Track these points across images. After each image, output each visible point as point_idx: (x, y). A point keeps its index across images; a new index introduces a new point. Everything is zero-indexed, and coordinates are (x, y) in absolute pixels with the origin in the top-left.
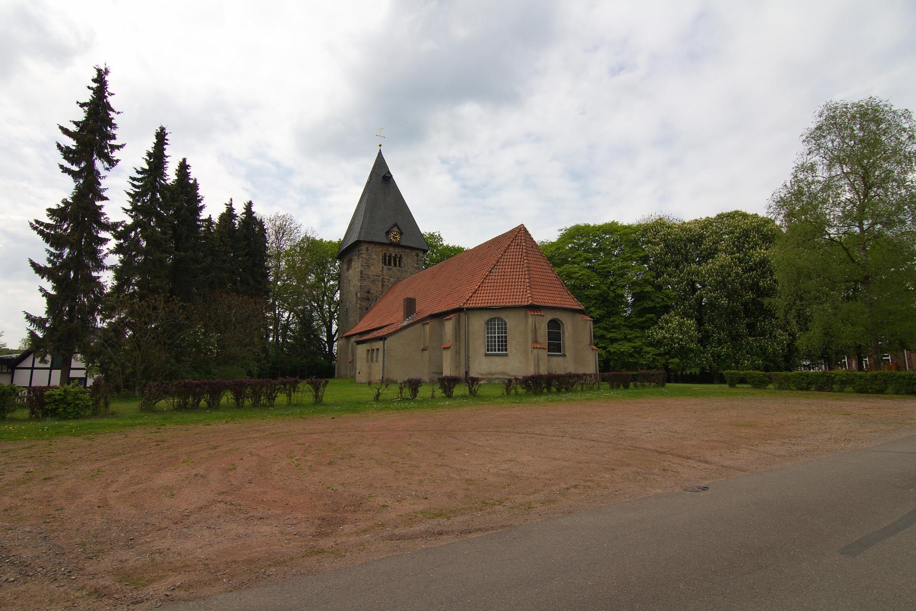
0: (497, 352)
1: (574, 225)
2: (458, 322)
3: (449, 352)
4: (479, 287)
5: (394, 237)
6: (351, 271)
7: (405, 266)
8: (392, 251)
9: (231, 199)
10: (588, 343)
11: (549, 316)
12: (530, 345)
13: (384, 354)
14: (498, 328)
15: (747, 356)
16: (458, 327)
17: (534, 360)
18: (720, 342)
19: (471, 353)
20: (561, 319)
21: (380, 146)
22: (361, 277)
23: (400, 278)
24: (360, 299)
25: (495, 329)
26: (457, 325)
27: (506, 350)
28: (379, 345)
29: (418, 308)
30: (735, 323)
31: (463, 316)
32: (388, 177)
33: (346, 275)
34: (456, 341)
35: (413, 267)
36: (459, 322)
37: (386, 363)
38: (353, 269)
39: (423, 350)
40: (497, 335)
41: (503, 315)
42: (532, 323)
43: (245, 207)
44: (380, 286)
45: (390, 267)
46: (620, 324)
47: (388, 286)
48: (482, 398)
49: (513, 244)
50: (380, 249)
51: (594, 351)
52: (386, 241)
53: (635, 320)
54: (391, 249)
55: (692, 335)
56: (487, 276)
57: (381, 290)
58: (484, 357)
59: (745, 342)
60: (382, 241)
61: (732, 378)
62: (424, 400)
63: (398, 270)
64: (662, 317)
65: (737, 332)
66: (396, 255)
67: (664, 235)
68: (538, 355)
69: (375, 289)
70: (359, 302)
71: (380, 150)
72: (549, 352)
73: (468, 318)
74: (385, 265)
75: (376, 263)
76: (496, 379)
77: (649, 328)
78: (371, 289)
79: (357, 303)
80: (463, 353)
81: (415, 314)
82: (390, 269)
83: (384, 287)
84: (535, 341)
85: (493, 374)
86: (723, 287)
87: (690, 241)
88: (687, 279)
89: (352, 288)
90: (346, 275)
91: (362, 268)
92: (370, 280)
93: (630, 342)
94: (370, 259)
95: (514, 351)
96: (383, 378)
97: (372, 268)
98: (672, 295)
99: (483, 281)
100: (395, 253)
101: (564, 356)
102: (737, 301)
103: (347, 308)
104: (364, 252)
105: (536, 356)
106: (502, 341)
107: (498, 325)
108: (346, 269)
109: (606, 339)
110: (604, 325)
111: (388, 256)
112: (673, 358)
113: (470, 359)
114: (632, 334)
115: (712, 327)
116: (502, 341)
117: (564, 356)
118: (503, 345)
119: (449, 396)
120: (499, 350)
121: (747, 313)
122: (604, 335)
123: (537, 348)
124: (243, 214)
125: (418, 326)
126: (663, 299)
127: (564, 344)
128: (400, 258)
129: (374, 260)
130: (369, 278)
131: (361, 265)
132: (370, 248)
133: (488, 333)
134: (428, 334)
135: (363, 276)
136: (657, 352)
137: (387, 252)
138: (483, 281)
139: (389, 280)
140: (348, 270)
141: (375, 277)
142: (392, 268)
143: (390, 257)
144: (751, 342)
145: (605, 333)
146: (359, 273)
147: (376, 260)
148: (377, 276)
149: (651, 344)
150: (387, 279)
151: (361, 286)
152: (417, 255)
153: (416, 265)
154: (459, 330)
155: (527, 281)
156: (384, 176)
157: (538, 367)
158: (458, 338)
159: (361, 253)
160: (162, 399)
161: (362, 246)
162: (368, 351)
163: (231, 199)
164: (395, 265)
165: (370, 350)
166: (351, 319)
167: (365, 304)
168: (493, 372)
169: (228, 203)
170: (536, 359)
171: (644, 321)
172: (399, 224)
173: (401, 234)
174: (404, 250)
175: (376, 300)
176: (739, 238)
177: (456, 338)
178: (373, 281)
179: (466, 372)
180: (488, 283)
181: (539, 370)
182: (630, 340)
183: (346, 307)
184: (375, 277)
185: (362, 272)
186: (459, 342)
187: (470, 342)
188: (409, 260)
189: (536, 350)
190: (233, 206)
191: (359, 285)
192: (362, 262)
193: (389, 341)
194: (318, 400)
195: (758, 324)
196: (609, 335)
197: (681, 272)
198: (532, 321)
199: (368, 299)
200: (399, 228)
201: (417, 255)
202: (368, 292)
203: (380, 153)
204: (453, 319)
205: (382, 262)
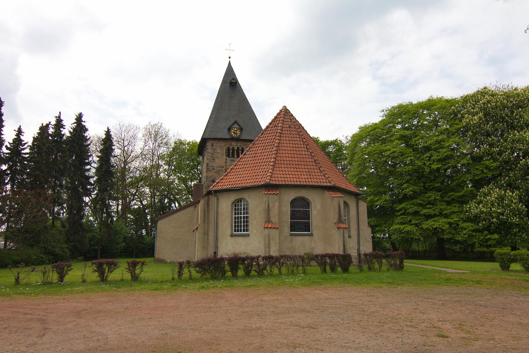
0: (242, 233)
1: (395, 104)
2: (208, 204)
5: (235, 132)
8: (235, 145)
9: (60, 113)
10: (335, 221)
11: (292, 195)
16: (206, 209)
17: (265, 240)
20: (309, 199)
21: (230, 58)
31: (213, 199)
41: (245, 195)
45: (233, 159)
46: (435, 199)
48: (142, 282)
50: (223, 144)
51: (342, 230)
52: (227, 137)
53: (453, 195)
55: (514, 209)
58: (230, 237)
60: (224, 137)
61: (503, 259)
62: (72, 284)
64: (481, 191)
66: (238, 148)
67: (484, 103)
68: (269, 235)
71: (230, 61)
72: (291, 231)
75: (220, 156)
77: (467, 203)
93: (448, 218)
94: (215, 153)
95: (255, 231)
97: (216, 160)
100: (237, 147)
101: (312, 235)
105: (267, 236)
109: (420, 215)
110: (420, 202)
111: (231, 149)
112: (492, 234)
114: (448, 210)
117: (312, 235)
118: (307, 227)
119: (103, 279)
120: (244, 231)
122: (419, 212)
124: (74, 123)
126: (482, 171)
127: (311, 222)
129: (218, 154)
130: (214, 169)
133: (235, 215)
136: (476, 227)
137: (230, 146)
141: (219, 168)
143: (233, 149)
145: (420, 209)
148: (221, 167)
149: (468, 220)
151: (207, 176)
154: (208, 212)
157: (269, 248)
158: (206, 219)
163: (60, 113)
169: (58, 116)
170: (267, 239)
171: (462, 196)
172: (238, 122)
173: (241, 130)
174: (245, 143)
177: (204, 220)
179: (215, 253)
181: (269, 251)
182: (446, 216)
184: (219, 168)
186: (208, 224)
189: (267, 230)
190: (62, 118)
194: (103, 279)
196: (425, 211)
203: (230, 66)
205: (226, 155)
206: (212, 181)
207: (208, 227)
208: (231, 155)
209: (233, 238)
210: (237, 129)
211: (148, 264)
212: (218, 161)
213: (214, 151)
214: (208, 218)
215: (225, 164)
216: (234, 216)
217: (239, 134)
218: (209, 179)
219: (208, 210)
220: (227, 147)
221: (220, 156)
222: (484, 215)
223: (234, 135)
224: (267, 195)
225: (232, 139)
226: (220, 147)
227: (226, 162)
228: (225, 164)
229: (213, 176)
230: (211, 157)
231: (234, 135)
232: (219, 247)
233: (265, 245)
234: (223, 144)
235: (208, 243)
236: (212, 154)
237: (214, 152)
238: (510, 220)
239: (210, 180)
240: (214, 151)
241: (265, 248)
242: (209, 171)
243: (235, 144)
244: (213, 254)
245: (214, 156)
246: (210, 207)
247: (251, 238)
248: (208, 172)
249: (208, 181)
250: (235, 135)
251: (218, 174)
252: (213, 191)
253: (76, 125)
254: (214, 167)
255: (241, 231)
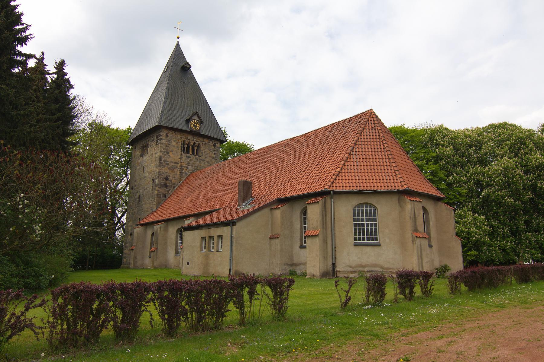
0: (366, 242)
3: (317, 241)
4: (342, 169)
5: (194, 125)
6: (146, 158)
7: (203, 156)
8: (191, 140)
9: (43, 53)
12: (409, 234)
13: (232, 242)
14: (367, 215)
15: (527, 249)
16: (324, 212)
18: (504, 238)
19: (338, 241)
21: (178, 38)
22: (160, 163)
23: (197, 167)
24: (158, 185)
25: (363, 215)
26: (324, 209)
27: (376, 240)
28: (225, 231)
29: (255, 191)
30: (515, 219)
32: (187, 67)
33: (139, 161)
34: (323, 228)
35: (210, 157)
36: (325, 207)
37: (235, 252)
38: (149, 154)
39: (271, 238)
40: (365, 222)
41: (373, 200)
42: (412, 210)
43: (56, 66)
44: (178, 173)
45: (188, 155)
47: (186, 174)
49: (367, 127)
50: (179, 136)
52: (186, 129)
54: (190, 137)
56: (348, 158)
57: (179, 177)
58: (352, 248)
59: (524, 236)
63: (197, 159)
65: (517, 228)
66: (194, 143)
69: (174, 176)
70: (157, 188)
73: (334, 202)
74: (184, 152)
75: (175, 149)
76: (368, 271)
78: (169, 176)
79: (153, 189)
80: (329, 243)
81: (251, 199)
82: (189, 157)
83: (182, 175)
84: (416, 230)
85: (364, 267)
86: (507, 187)
87: (470, 146)
88: (474, 179)
89: (147, 174)
90: (139, 161)
91: (161, 154)
92: (169, 166)
95: (387, 240)
96: (230, 270)
97: (171, 154)
98: (463, 193)
99: (345, 163)
100: (193, 142)
102: (518, 199)
103: (140, 195)
104: (164, 138)
105: (419, 246)
106: (372, 229)
107: (366, 211)
108: (139, 156)
111: (186, 144)
113: (337, 249)
115: (497, 223)
116: (372, 229)
120: (368, 240)
121: (526, 212)
123: (420, 237)
125: (266, 211)
128: (198, 147)
130: (168, 164)
131: (161, 151)
132: (169, 135)
134: (280, 220)
135: (161, 163)
138: (345, 163)
139: (187, 168)
140: (142, 156)
141: (173, 164)
142: (190, 156)
144: (530, 237)
146: (158, 159)
147: (175, 147)
148: (175, 163)
150: (185, 167)
151: (159, 172)
152: (214, 145)
153: (213, 155)
154: (326, 216)
155: (394, 165)
156: (183, 66)
159: (161, 139)
160: (117, 333)
161: (161, 131)
162: (202, 238)
163: (43, 53)
164: (193, 153)
165: (207, 239)
166: (146, 206)
167: (163, 191)
168: (363, 264)
170: (419, 249)
172: (199, 112)
173: (201, 123)
174: (202, 139)
175: (174, 187)
176: (515, 144)
178: (172, 168)
179: (334, 265)
180: (351, 165)
183: (138, 194)
185: (160, 158)
187: (337, 230)
188: (206, 149)
190: (45, 62)
191: (158, 171)
192: (161, 148)
193: (238, 225)
195: (533, 221)
197: (468, 172)
198: (412, 208)
199: (166, 186)
200: (199, 117)
201: (214, 145)
202: (167, 179)
203: (178, 45)
204: (320, 203)
205: (181, 150)
206: (165, 179)
207: (326, 233)
208: (185, 151)
209: (357, 247)
210: (196, 122)
211: (358, 280)
212: (173, 156)
213: (169, 143)
214: (326, 223)
215: (180, 160)
216: (377, 222)
217: (198, 128)
218: (162, 175)
219: (325, 213)
220: (183, 140)
221: (175, 149)
222: (464, 234)
223: (193, 128)
224: (413, 202)
225: (192, 133)
226: (175, 139)
227: (181, 158)
228: (180, 160)
229: (167, 173)
230: (165, 149)
231: (193, 128)
232: (337, 257)
233: (418, 256)
234: (179, 136)
235: (327, 252)
236: (166, 146)
237: (168, 144)
238: (482, 239)
239: (163, 177)
240: (169, 143)
241: (418, 259)
242: (162, 165)
243: (191, 138)
244: (332, 265)
245: (168, 149)
246: (327, 210)
247: (383, 248)
248: (162, 167)
249: (161, 178)
250: (194, 128)
251: (172, 171)
252: (332, 192)
253: (56, 76)
254: (168, 162)
255: (364, 240)
